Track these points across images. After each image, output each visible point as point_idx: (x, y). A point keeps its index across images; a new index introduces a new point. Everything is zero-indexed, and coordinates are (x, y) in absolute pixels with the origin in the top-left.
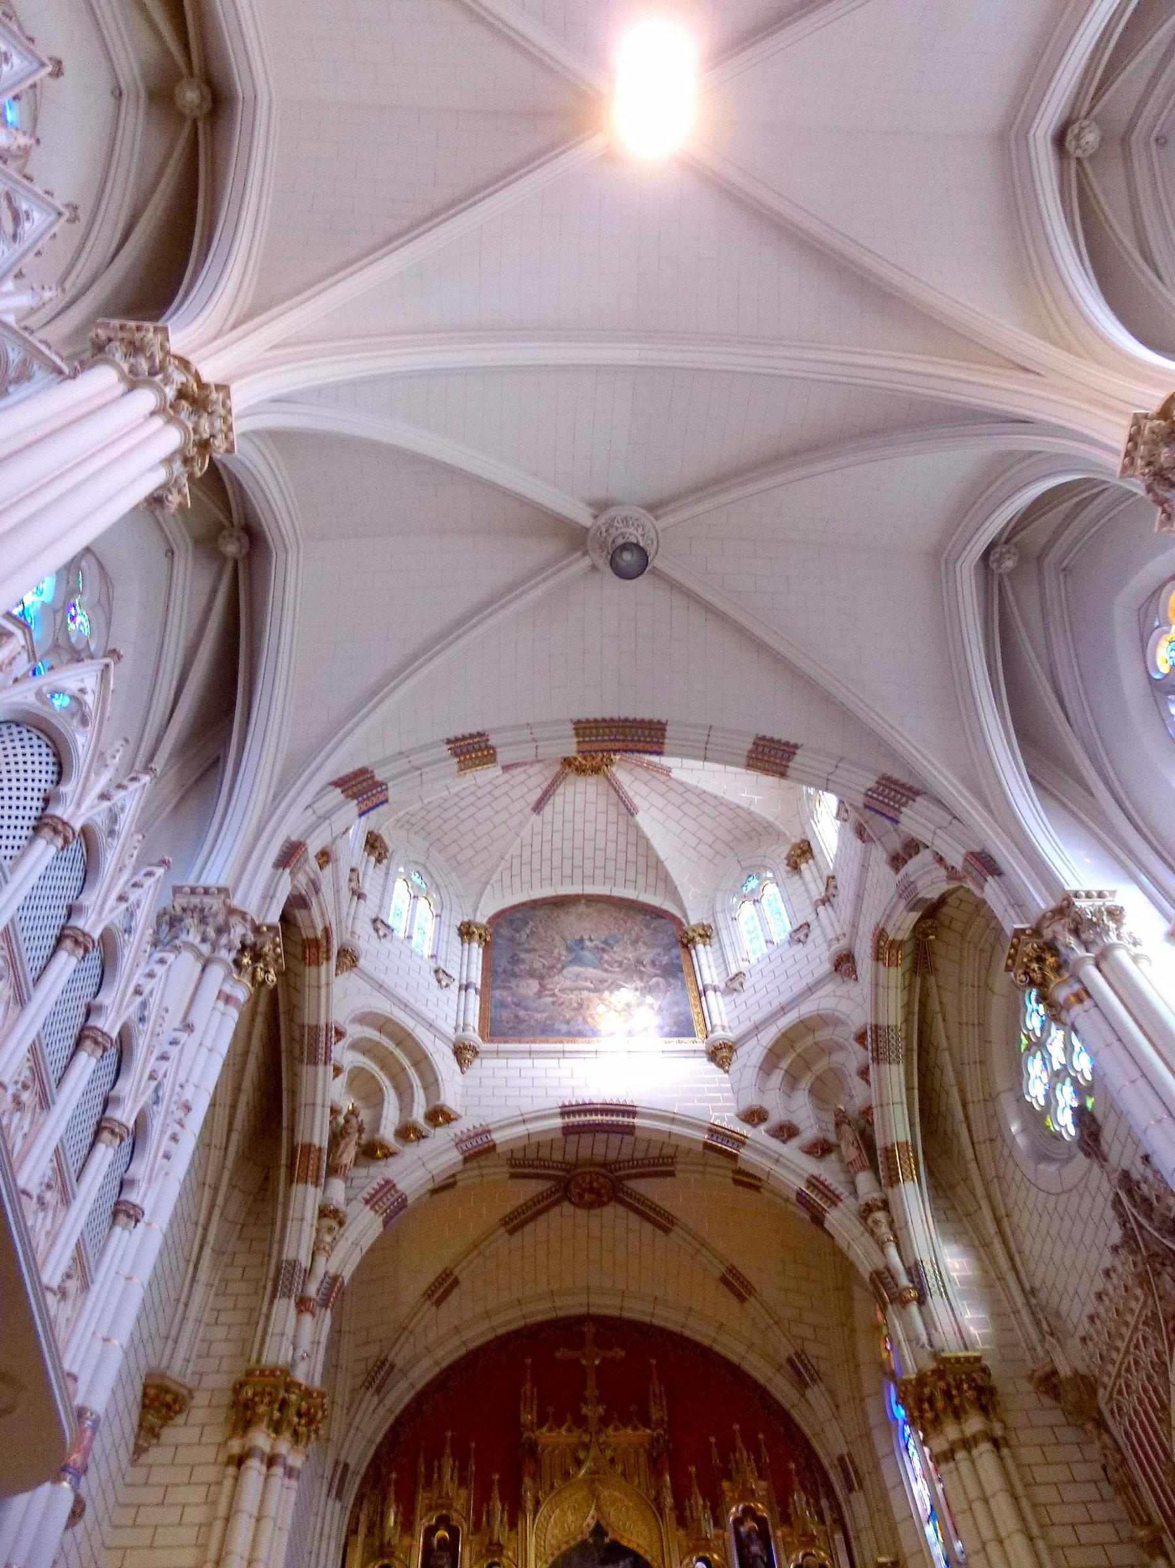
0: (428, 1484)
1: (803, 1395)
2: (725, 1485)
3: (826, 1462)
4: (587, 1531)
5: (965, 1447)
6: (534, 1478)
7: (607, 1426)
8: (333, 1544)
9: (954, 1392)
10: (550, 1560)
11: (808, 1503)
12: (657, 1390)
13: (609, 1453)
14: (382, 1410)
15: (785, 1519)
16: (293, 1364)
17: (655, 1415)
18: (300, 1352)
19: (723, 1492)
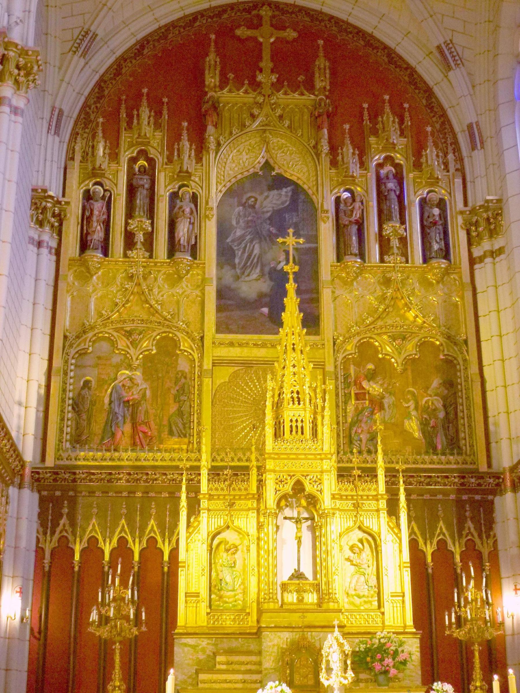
0: (130, 124)
1: (446, 77)
2: (372, 140)
3: (457, 128)
4: (258, 166)
5: (492, 256)
6: (216, 126)
7: (278, 91)
8: (55, 166)
9: (492, 220)
10: (228, 185)
11: (437, 156)
12: (322, 66)
13: (279, 112)
14: (88, 71)
15: (418, 165)
16: (9, 28)
17: (319, 84)
18: (14, 19)
19: (370, 146)
